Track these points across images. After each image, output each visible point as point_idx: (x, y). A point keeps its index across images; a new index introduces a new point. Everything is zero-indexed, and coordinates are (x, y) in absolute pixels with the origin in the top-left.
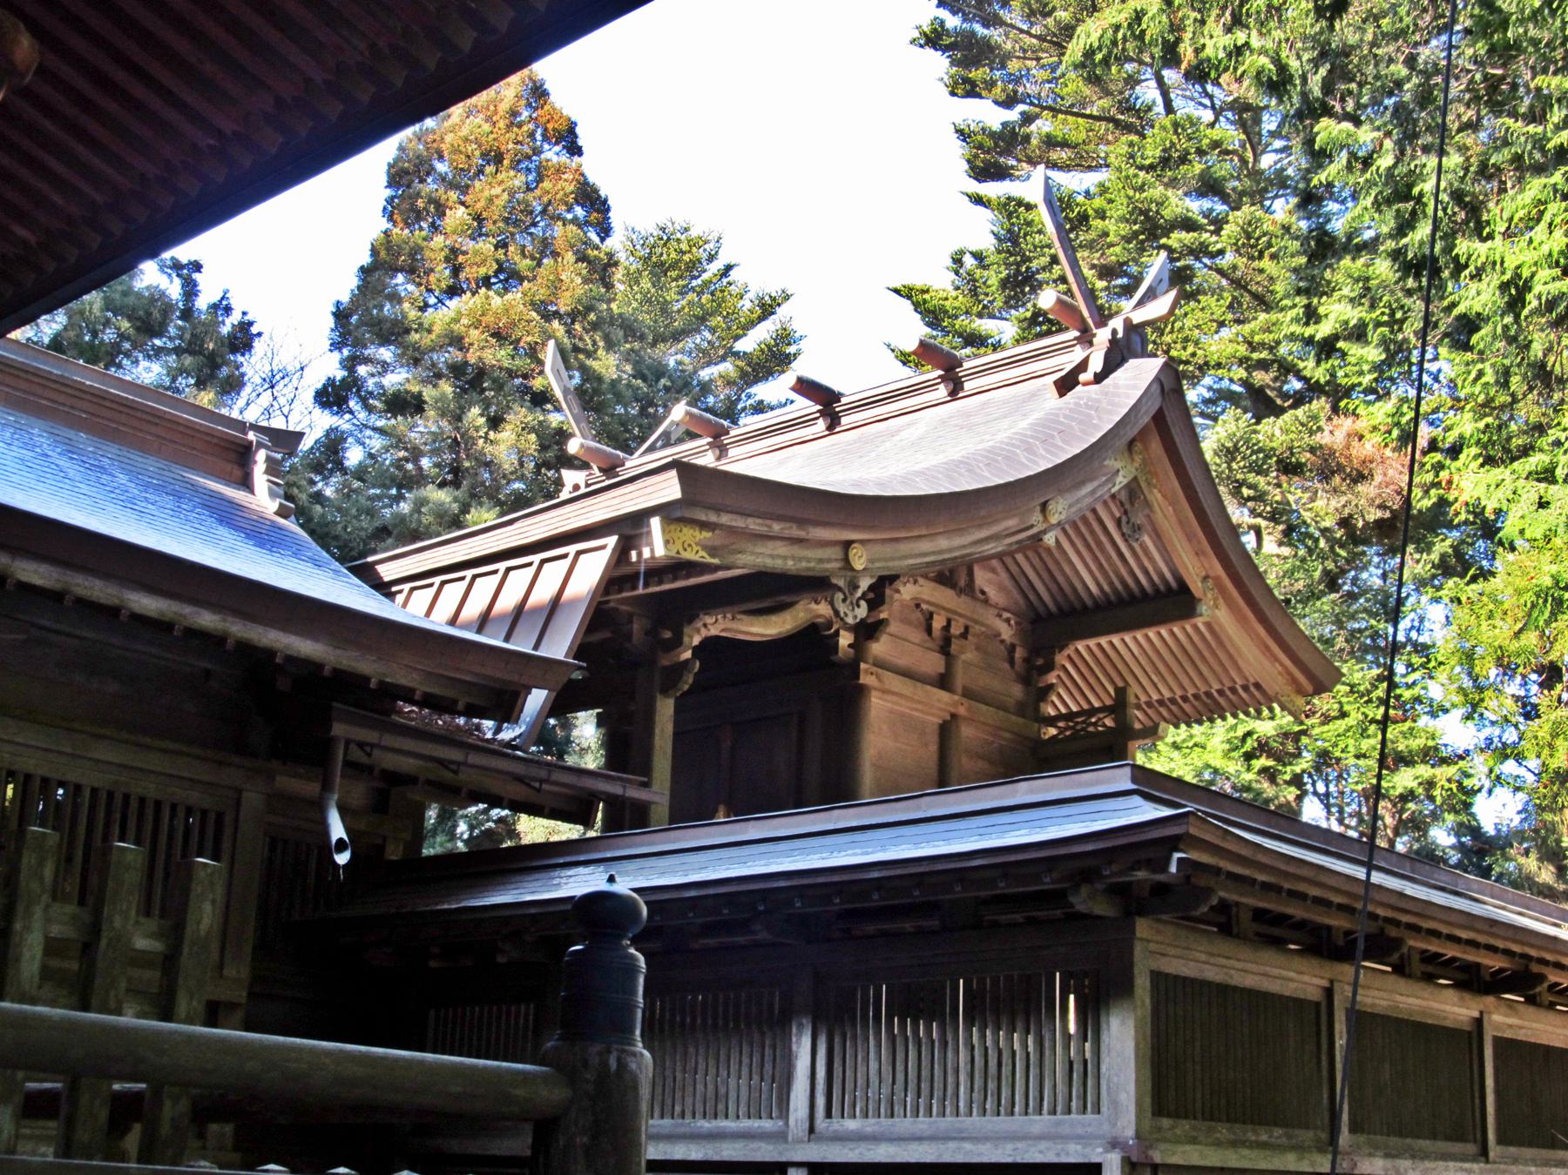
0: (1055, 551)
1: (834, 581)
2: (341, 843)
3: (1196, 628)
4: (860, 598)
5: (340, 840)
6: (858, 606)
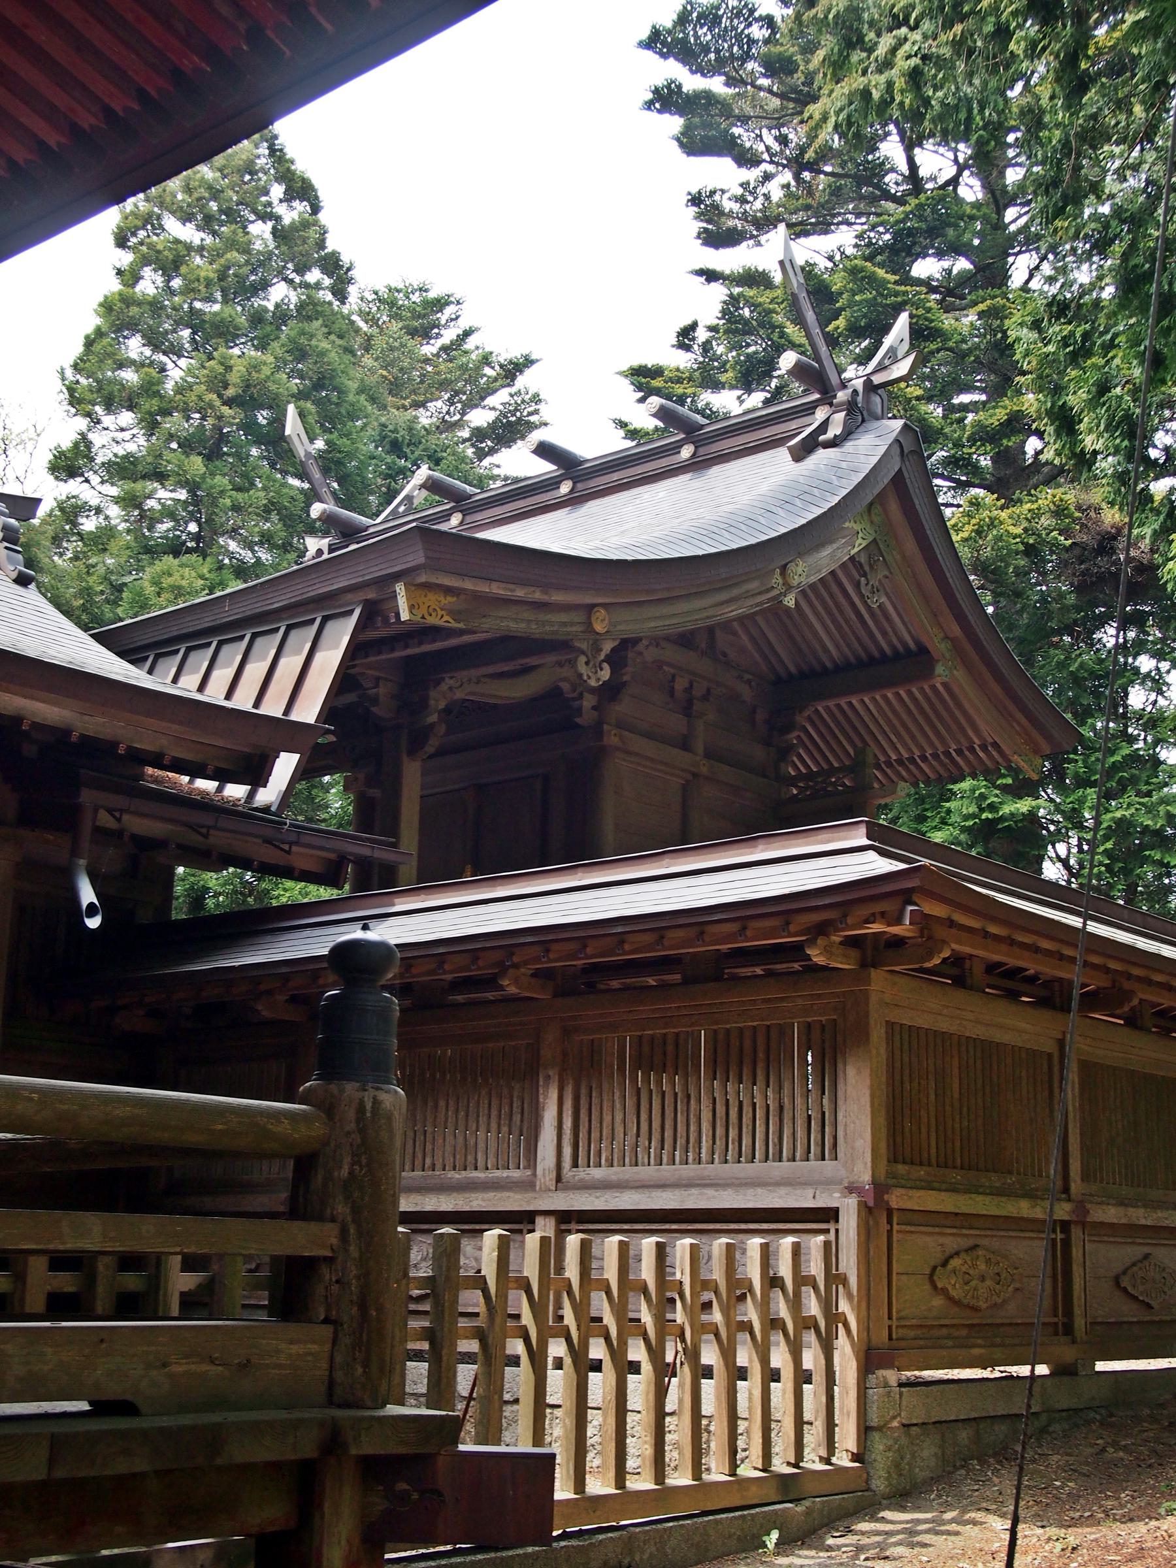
0: (795, 614)
1: (577, 644)
2: (92, 910)
3: (934, 688)
4: (603, 661)
5: (91, 905)
6: (601, 669)
